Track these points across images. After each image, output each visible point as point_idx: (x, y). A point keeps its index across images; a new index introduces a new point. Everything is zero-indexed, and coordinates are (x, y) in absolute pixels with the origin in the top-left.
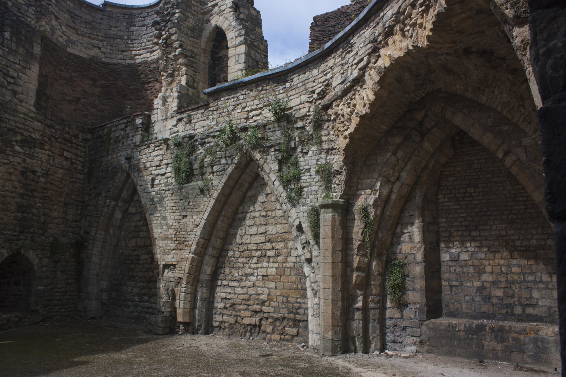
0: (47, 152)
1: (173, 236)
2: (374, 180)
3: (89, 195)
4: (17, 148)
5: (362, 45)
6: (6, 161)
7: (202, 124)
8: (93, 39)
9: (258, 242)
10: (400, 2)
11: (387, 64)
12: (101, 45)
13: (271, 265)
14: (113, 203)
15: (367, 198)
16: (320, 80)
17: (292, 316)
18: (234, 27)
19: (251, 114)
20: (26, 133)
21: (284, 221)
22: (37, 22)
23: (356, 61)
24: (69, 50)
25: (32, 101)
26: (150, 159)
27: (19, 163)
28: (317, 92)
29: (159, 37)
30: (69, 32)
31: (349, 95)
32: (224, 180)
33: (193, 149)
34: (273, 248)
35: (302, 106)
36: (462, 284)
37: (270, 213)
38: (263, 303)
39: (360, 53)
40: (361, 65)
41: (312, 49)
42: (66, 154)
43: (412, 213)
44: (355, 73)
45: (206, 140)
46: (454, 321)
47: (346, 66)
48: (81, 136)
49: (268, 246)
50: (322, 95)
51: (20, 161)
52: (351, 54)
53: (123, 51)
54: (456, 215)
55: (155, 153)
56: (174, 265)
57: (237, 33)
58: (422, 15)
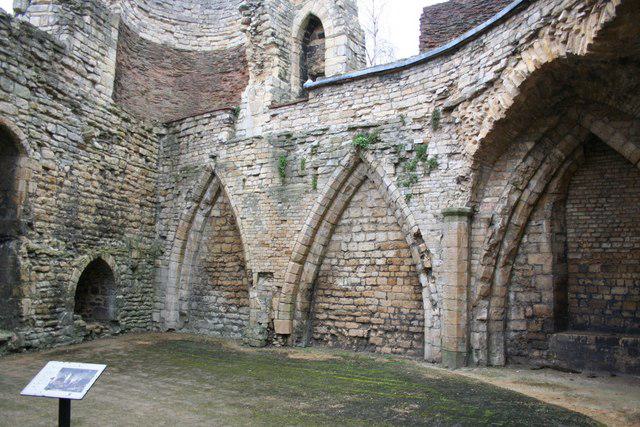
0: (124, 148)
1: (270, 242)
2: (503, 188)
3: (165, 196)
4: (97, 144)
5: (498, 46)
6: (86, 159)
7: (299, 121)
8: (165, 22)
9: (367, 249)
10: (553, 5)
11: (532, 69)
12: (173, 29)
13: (381, 274)
14: (195, 205)
15: (493, 204)
16: (442, 80)
17: (405, 328)
18: (333, 16)
19: (359, 113)
20: (104, 127)
21: (397, 228)
22: (111, 4)
23: (490, 63)
24: (141, 35)
25: (110, 92)
26: (240, 158)
27: (99, 161)
28: (438, 92)
29: (248, 23)
30: (140, 14)
31: (481, 98)
32: (330, 183)
33: (291, 148)
34: (384, 256)
35: (419, 106)
36: (591, 297)
37: (380, 219)
38: (372, 314)
39: (496, 55)
40: (498, 67)
41: (425, 44)
42: (141, 150)
43: (540, 222)
44: (490, 76)
45: (307, 140)
46: (583, 335)
47: (476, 67)
48: (156, 131)
49: (378, 254)
50: (444, 96)
51: (99, 158)
52: (484, 55)
53: (198, 37)
54: (586, 226)
55: (246, 152)
56: (271, 274)
57: (335, 22)
58: (581, 21)
